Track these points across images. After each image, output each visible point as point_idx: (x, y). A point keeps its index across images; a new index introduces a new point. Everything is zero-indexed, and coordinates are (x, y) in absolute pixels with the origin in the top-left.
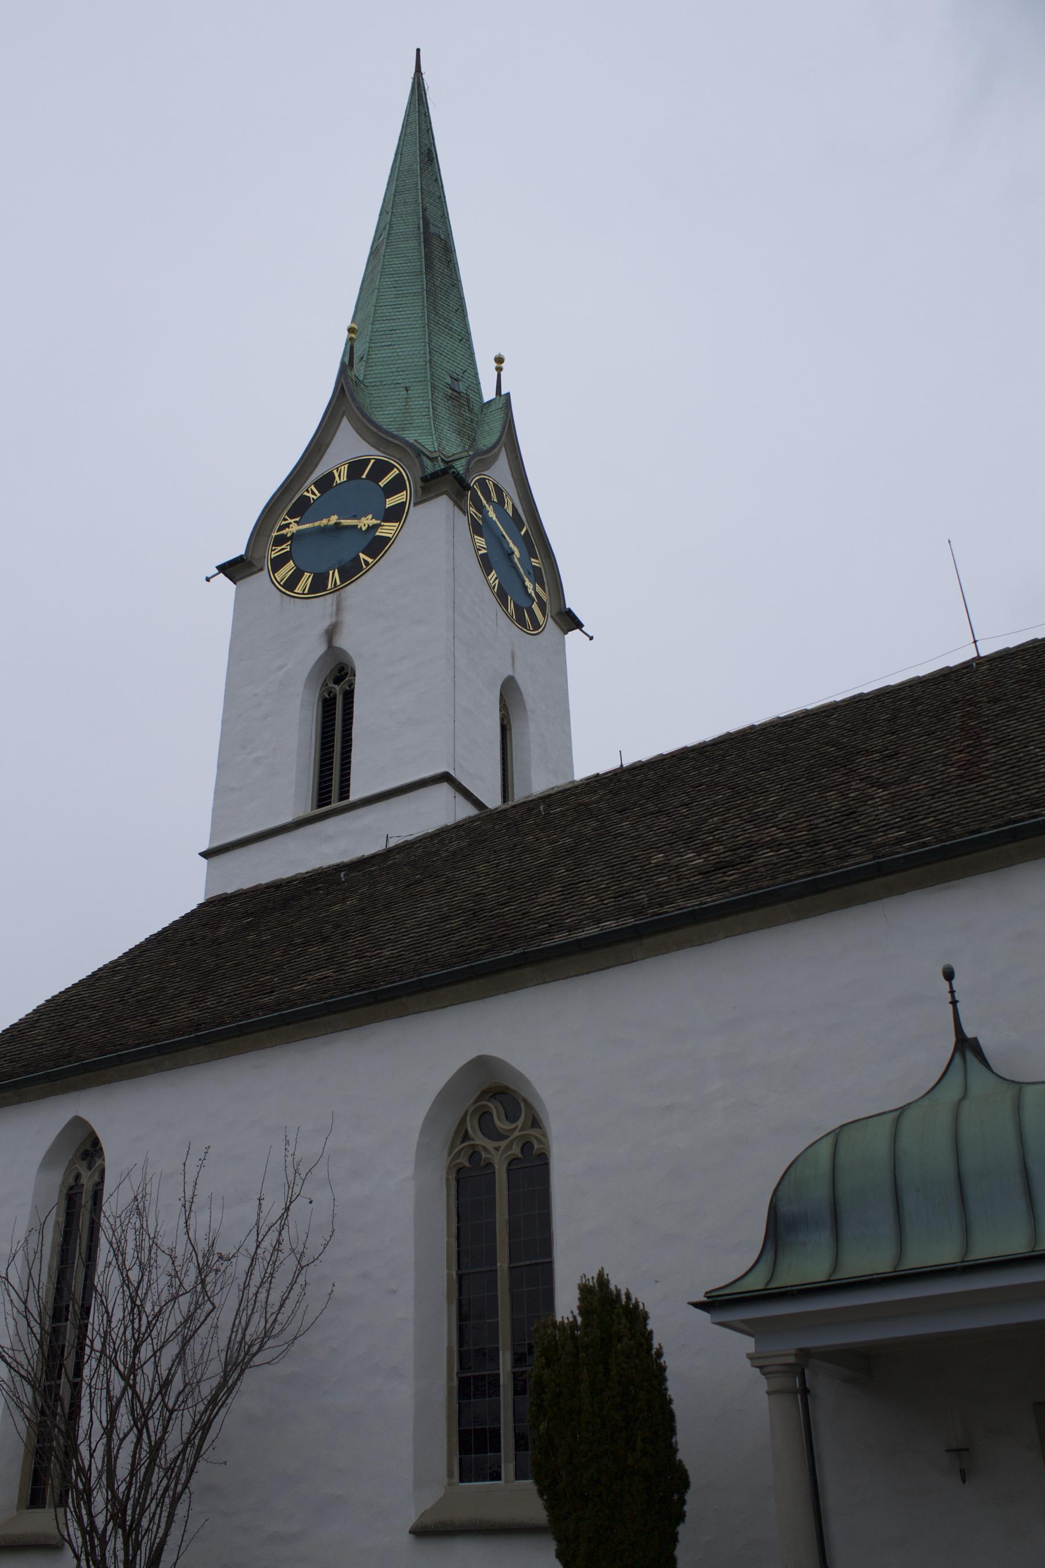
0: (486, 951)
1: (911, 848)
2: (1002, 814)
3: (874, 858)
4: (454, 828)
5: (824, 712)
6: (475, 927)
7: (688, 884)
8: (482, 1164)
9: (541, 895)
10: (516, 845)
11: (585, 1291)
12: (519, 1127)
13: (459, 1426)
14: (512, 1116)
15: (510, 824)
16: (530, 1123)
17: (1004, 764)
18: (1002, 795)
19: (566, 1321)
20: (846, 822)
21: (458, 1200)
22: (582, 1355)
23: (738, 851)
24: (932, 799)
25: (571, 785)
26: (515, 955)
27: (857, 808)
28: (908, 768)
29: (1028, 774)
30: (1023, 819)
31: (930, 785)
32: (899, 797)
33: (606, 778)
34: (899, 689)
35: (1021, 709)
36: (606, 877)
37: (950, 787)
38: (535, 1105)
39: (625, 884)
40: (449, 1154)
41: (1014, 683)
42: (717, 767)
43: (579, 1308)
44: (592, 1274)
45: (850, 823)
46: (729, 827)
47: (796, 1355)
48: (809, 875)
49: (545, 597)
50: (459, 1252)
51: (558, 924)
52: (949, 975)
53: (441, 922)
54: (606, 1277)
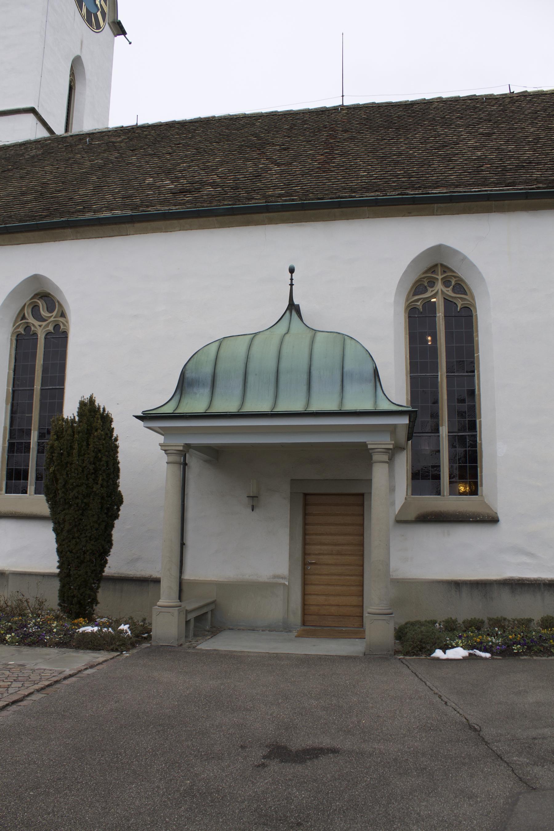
0: (46, 216)
1: (286, 201)
2: (336, 192)
3: (266, 202)
4: (35, 142)
5: (255, 117)
6: (40, 202)
7: (164, 198)
8: (31, 333)
9: (81, 190)
10: (70, 158)
11: (82, 404)
12: (54, 316)
13: (7, 466)
14: (50, 309)
15: (68, 146)
16: (60, 314)
17: (342, 166)
18: (338, 183)
19: (69, 418)
20: (254, 180)
21: (16, 351)
22: (76, 436)
23: (194, 185)
24: (302, 177)
25: (106, 130)
26: (62, 221)
27: (262, 173)
28: (293, 158)
29: (354, 174)
30: (346, 197)
31: (302, 169)
32: (284, 173)
33: (127, 129)
34: (297, 113)
35: (358, 139)
36: (119, 186)
37: (312, 173)
38: (64, 305)
39: (129, 192)
40: (14, 326)
41: (357, 124)
42: (190, 135)
43: (78, 412)
44: (87, 396)
45: (257, 181)
46: (191, 171)
47: (183, 446)
48: (230, 205)
49: (106, 9)
50: (14, 378)
51: (89, 208)
52: (292, 271)
53: (21, 196)
54: (94, 398)
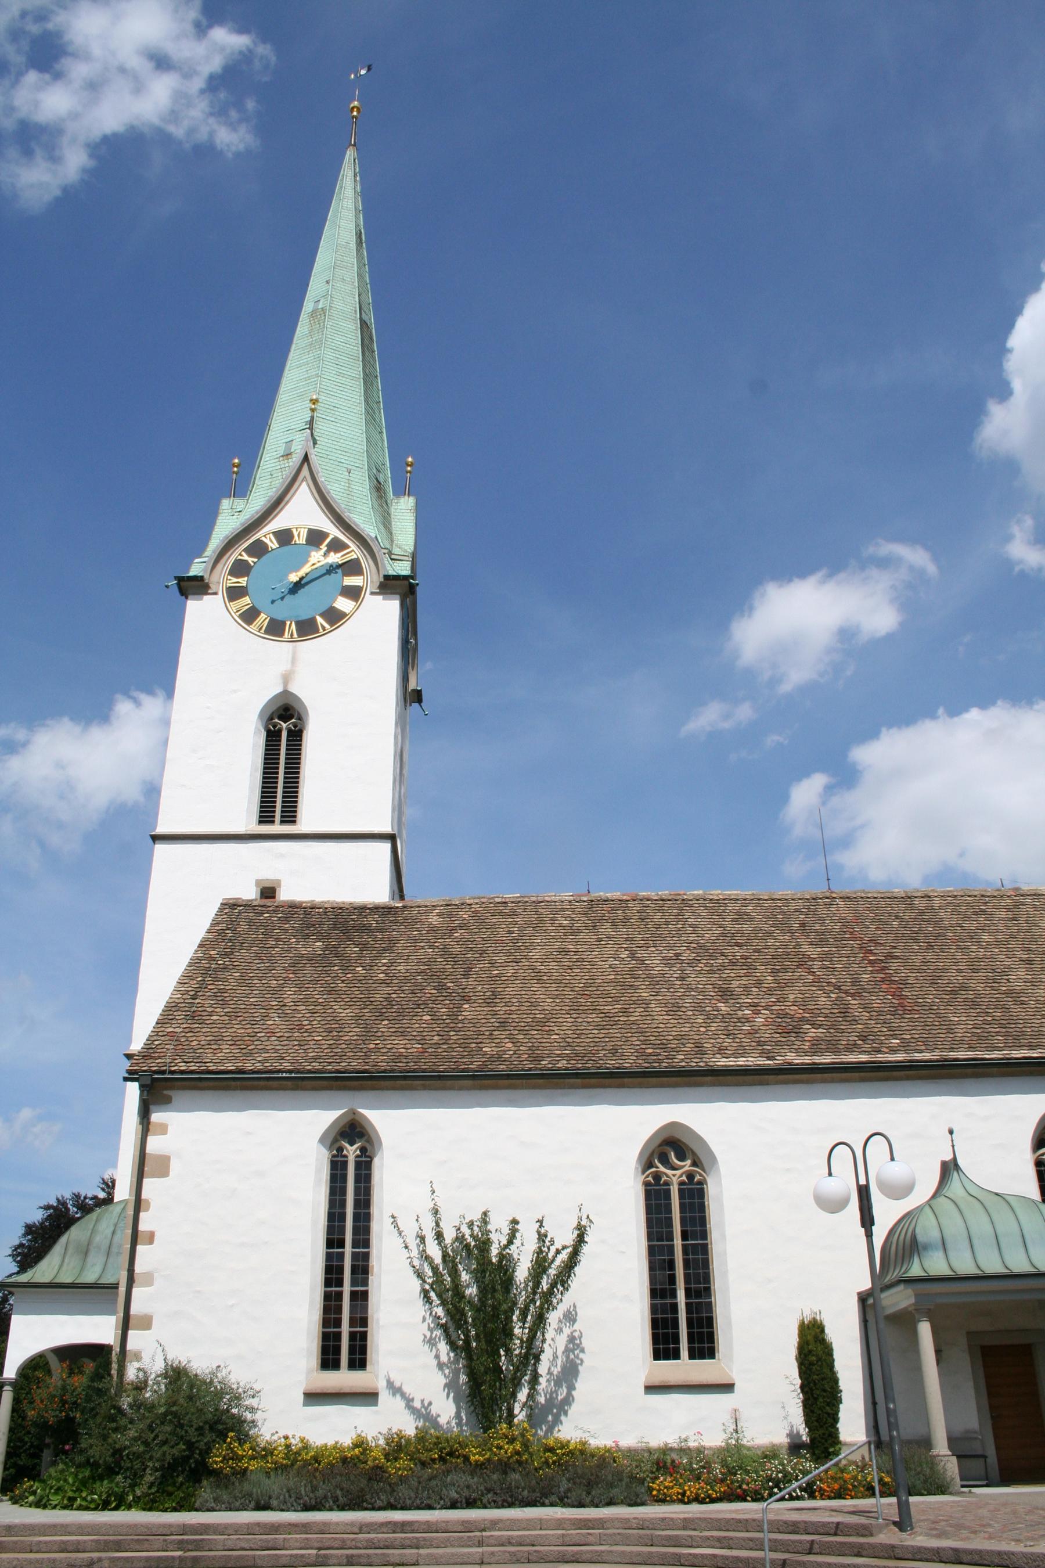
14: (681, 1157)
52: (951, 1132)
